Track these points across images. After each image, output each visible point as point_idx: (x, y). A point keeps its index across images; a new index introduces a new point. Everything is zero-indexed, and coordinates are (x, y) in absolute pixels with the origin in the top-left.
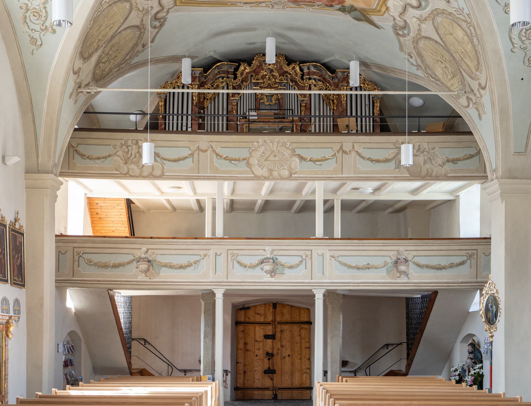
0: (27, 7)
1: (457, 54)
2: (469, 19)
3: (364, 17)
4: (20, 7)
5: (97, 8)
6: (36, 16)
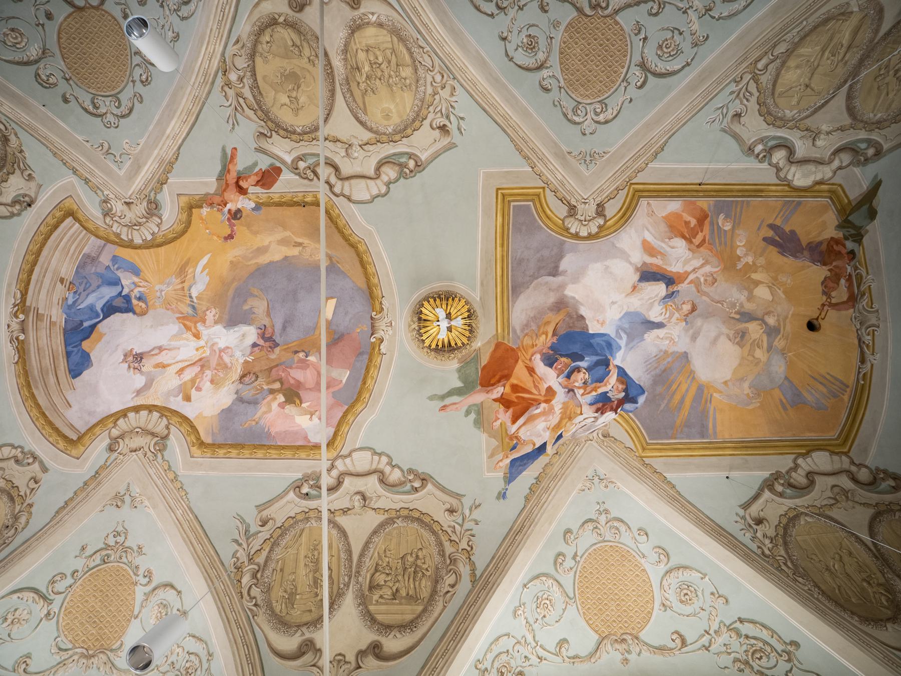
0: (740, 661)
1: (846, 58)
2: (744, 76)
3: (861, 206)
4: (740, 671)
5: (772, 565)
6: (761, 657)
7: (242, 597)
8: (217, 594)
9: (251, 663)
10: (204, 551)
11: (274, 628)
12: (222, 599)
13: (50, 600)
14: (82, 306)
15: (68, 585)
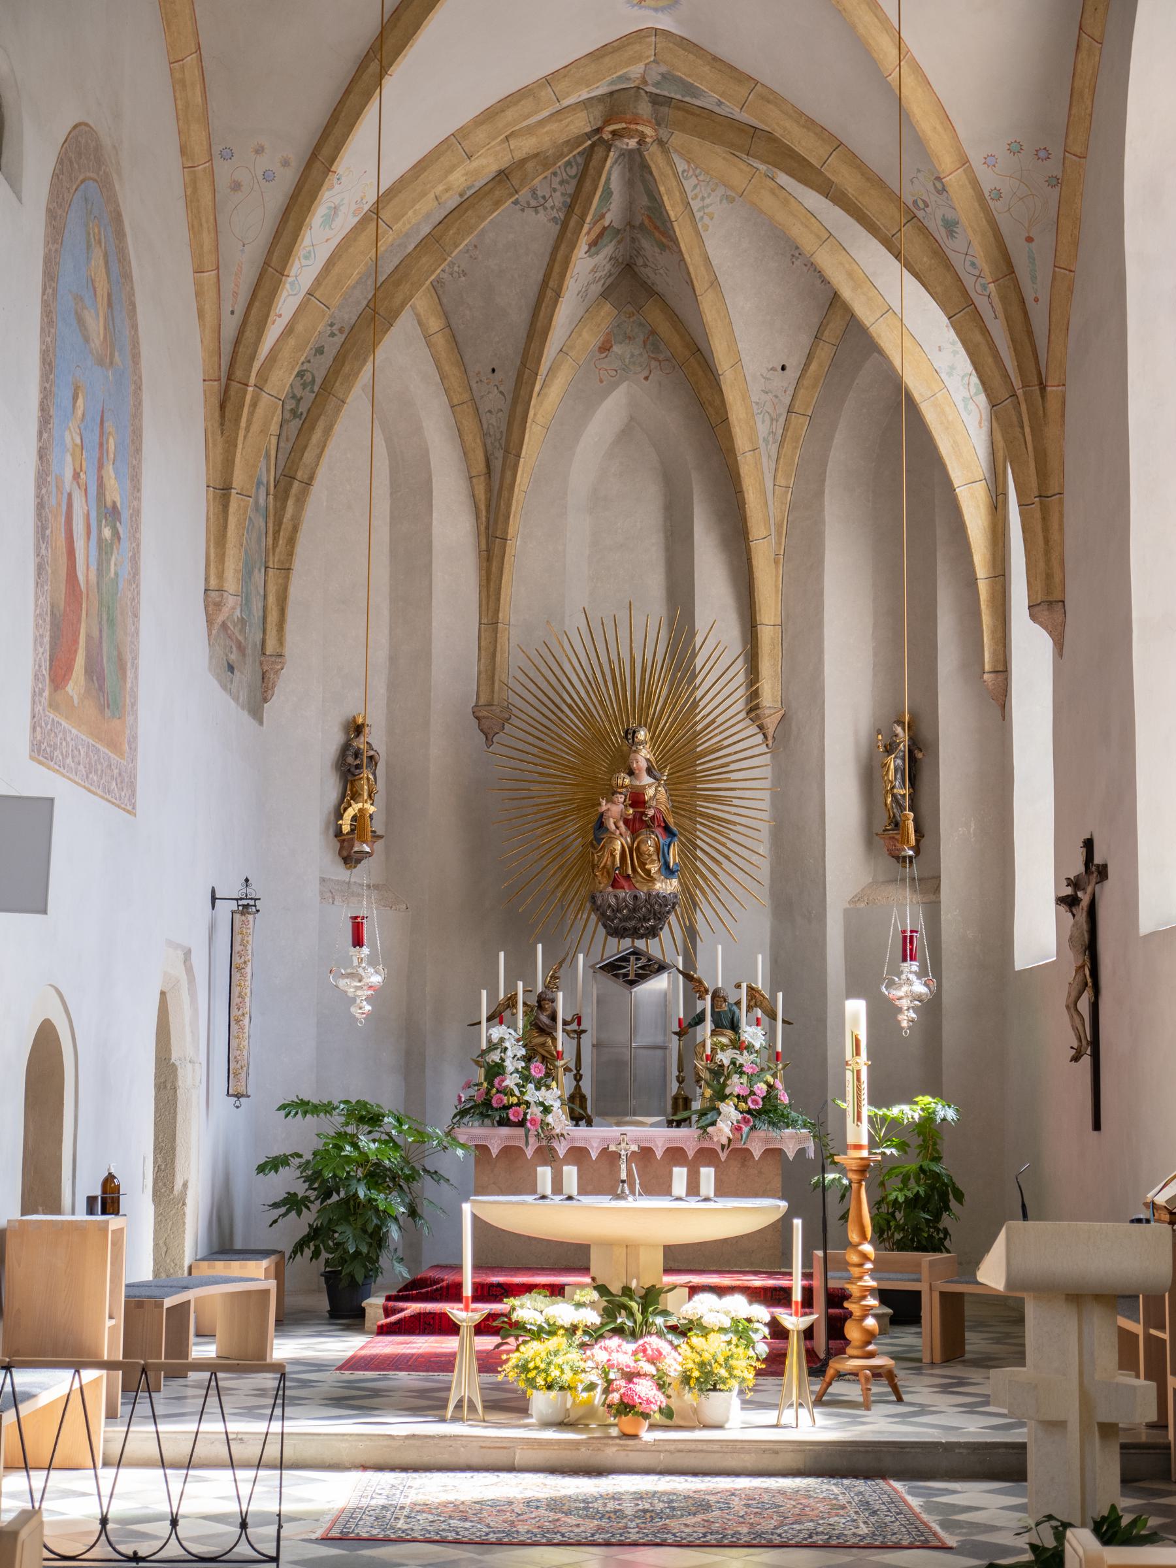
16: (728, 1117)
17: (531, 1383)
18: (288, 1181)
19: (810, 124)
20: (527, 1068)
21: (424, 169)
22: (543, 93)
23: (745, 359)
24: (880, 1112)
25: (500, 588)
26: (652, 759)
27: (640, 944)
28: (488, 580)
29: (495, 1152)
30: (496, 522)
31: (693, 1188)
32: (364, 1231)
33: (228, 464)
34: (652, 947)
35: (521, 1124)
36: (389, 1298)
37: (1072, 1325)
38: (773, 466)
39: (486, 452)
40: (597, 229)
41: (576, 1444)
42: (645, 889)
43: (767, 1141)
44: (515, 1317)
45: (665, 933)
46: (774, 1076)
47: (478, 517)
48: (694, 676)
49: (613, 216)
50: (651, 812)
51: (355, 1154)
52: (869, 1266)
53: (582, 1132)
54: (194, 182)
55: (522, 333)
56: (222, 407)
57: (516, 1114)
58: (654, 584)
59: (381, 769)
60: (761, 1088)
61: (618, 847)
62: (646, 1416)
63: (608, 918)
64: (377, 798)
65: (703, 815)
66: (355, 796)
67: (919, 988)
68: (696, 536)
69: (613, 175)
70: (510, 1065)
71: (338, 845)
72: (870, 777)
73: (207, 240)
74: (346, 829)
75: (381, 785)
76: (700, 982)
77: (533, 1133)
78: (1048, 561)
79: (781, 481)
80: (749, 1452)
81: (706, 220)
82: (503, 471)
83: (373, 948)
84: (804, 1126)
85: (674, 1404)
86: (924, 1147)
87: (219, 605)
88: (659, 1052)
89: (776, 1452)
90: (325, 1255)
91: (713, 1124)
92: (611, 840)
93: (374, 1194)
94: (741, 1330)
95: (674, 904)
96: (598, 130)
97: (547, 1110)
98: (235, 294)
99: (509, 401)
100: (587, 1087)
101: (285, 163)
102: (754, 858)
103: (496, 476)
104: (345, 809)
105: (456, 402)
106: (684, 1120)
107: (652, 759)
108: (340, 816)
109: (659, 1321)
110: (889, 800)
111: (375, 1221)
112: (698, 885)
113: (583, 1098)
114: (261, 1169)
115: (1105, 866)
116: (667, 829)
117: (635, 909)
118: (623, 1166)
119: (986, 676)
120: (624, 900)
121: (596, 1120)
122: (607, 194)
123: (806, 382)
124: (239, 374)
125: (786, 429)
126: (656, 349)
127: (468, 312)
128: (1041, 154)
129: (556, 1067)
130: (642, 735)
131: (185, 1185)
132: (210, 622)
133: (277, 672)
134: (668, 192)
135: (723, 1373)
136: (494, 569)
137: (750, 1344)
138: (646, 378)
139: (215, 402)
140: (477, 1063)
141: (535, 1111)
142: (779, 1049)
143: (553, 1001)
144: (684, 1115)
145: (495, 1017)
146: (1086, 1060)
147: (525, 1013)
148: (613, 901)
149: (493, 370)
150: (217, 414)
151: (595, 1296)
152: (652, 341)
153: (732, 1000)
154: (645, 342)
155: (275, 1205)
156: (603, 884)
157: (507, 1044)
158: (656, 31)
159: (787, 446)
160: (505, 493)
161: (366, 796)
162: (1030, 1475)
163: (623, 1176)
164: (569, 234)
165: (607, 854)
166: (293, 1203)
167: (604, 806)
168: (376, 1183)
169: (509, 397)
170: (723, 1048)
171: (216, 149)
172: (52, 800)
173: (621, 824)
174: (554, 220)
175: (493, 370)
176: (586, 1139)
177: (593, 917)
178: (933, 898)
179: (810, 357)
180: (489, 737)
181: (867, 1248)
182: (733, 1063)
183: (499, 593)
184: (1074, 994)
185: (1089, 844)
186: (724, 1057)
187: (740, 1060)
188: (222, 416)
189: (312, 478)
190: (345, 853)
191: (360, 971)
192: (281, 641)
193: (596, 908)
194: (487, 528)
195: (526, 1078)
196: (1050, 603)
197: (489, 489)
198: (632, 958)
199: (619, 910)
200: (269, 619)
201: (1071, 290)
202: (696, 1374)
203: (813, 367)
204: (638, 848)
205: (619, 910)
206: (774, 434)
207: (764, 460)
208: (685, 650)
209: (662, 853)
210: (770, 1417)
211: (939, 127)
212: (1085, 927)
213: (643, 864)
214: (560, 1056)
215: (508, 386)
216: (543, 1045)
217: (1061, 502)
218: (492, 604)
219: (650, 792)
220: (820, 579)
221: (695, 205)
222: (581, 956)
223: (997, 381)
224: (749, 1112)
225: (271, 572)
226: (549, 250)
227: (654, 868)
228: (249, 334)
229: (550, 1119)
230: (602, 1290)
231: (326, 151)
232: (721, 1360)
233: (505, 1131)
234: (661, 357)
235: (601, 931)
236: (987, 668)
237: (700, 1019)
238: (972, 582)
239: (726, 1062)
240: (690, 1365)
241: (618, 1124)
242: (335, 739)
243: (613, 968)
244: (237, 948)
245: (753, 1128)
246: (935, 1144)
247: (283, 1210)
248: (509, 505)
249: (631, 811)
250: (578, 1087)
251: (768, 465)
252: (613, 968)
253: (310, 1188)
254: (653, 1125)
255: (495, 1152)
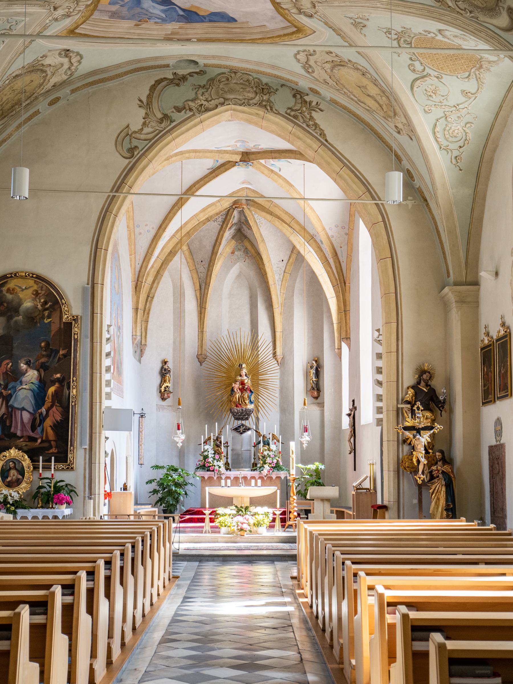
7: (462, 14)
8: (453, 24)
9: (504, 46)
10: (417, 9)
11: (492, 17)
12: (458, 24)
13: (427, 74)
14: (164, 16)
15: (420, 64)
16: (266, 468)
17: (221, 525)
18: (154, 486)
19: (286, 213)
20: (214, 456)
21: (187, 224)
22: (218, 204)
23: (272, 259)
24: (305, 467)
25: (204, 322)
26: (247, 372)
27: (243, 422)
28: (201, 319)
29: (206, 478)
30: (203, 303)
31: (256, 485)
32: (174, 498)
33: (137, 302)
34: (246, 423)
35: (213, 471)
36: (181, 515)
37: (322, 504)
38: (280, 287)
39: (200, 283)
40: (231, 224)
41: (231, 537)
42: (245, 407)
43: (277, 475)
44: (217, 512)
45: (250, 419)
46: (279, 458)
47: (197, 302)
48: (258, 348)
49: (235, 220)
50: (246, 387)
51: (172, 479)
52: (295, 501)
53: (228, 473)
54: (130, 234)
55: (210, 252)
56: (136, 288)
57: (212, 468)
58: (247, 319)
59: (171, 373)
60: (275, 461)
61: (238, 396)
62: (246, 531)
63: (235, 415)
64: (170, 381)
65: (260, 384)
66: (165, 381)
67: (308, 439)
68: (259, 307)
69: (236, 213)
70: (210, 456)
71: (160, 395)
72: (307, 375)
73: (133, 247)
74: (163, 391)
75: (172, 378)
76: (259, 433)
77: (216, 473)
78: (346, 328)
79: (282, 291)
80: (267, 538)
81: (261, 225)
82: (205, 289)
83: (182, 430)
84: (286, 471)
85: (252, 529)
86: (316, 475)
87: (135, 339)
88: (249, 452)
89: (273, 538)
90: (163, 505)
91: (263, 470)
92: (236, 394)
93: (177, 489)
94: (266, 514)
95: (253, 411)
96: (232, 206)
97: (220, 467)
98: (139, 259)
99: (206, 270)
100: (229, 461)
101: (153, 228)
102: (275, 398)
103: (203, 291)
104: (162, 385)
105: (191, 269)
106: (255, 469)
107: (247, 372)
108: (161, 387)
109: (249, 513)
110: (311, 382)
111: (177, 496)
112: (259, 406)
113: (228, 464)
114: (147, 483)
115: (356, 407)
116: (251, 391)
117: (242, 413)
118: (241, 480)
119: (336, 350)
120: (239, 410)
121: (232, 470)
122: (234, 217)
123: (289, 264)
124: (140, 279)
125: (283, 277)
126: (247, 253)
127: (195, 245)
128: (343, 228)
129: (221, 456)
130: (244, 366)
131: (130, 487)
132: (133, 343)
133: (145, 349)
134: (250, 219)
135: (262, 523)
136: (202, 316)
137: (268, 517)
138: (244, 261)
139: (134, 287)
140: (201, 455)
141: (217, 468)
142: (280, 451)
143: (220, 438)
144: (255, 468)
145: (205, 442)
146: (353, 454)
147: (213, 442)
148: (236, 411)
149: (202, 261)
150: (135, 290)
151: (235, 508)
152: (246, 251)
153: (268, 438)
154: (244, 251)
155: (150, 492)
156: (233, 406)
157: (209, 450)
158: (247, 188)
159: (284, 282)
160: (205, 296)
161: (168, 381)
162: (447, 660)
163: (241, 482)
164: (223, 229)
165: (234, 398)
166: (155, 492)
167: (234, 385)
168: (177, 486)
169: (206, 269)
170: (266, 450)
171: (135, 226)
172: (111, 399)
173: (238, 390)
174: (219, 224)
175: (202, 261)
176: (230, 475)
177: (231, 415)
178: (323, 409)
179: (290, 257)
180: (201, 363)
181: (295, 497)
182: (268, 454)
183: (204, 323)
184: (350, 438)
185: (353, 401)
186: (265, 453)
187: (270, 454)
188: (136, 290)
189: (154, 296)
190: (162, 397)
191: (180, 436)
192: (146, 341)
193: (231, 412)
194: (200, 305)
195: (214, 459)
196: (347, 338)
197: (201, 294)
198: (241, 426)
199: (238, 413)
200: (142, 335)
201: (351, 260)
202: (256, 523)
203: (291, 260)
204: (243, 396)
205: (238, 413)
206: (280, 278)
207: (277, 286)
208: (255, 341)
209: (249, 397)
210: (273, 533)
211: (317, 222)
212: (352, 421)
213: (244, 401)
214: (222, 453)
215: (206, 266)
216: (218, 450)
217: (349, 313)
218: (202, 326)
219: (246, 381)
220: (293, 319)
221: (257, 221)
222: (228, 426)
223: (334, 280)
224: (272, 467)
225: (143, 322)
226: (218, 232)
227: (247, 402)
228: (143, 270)
229: (220, 469)
230: (236, 507)
231: (163, 226)
232: (262, 520)
233: (209, 473)
234: (249, 255)
235: (233, 418)
236: (336, 348)
237: (259, 443)
238: (333, 324)
239: (266, 454)
240: (255, 521)
241: (238, 471)
242: (159, 365)
243: (236, 429)
244: (140, 426)
245: (273, 471)
246: (319, 475)
247: (152, 493)
248: (206, 299)
249: (241, 386)
250: (227, 461)
251: (278, 287)
252: (236, 429)
253: (160, 488)
254: (247, 471)
255: (206, 478)
